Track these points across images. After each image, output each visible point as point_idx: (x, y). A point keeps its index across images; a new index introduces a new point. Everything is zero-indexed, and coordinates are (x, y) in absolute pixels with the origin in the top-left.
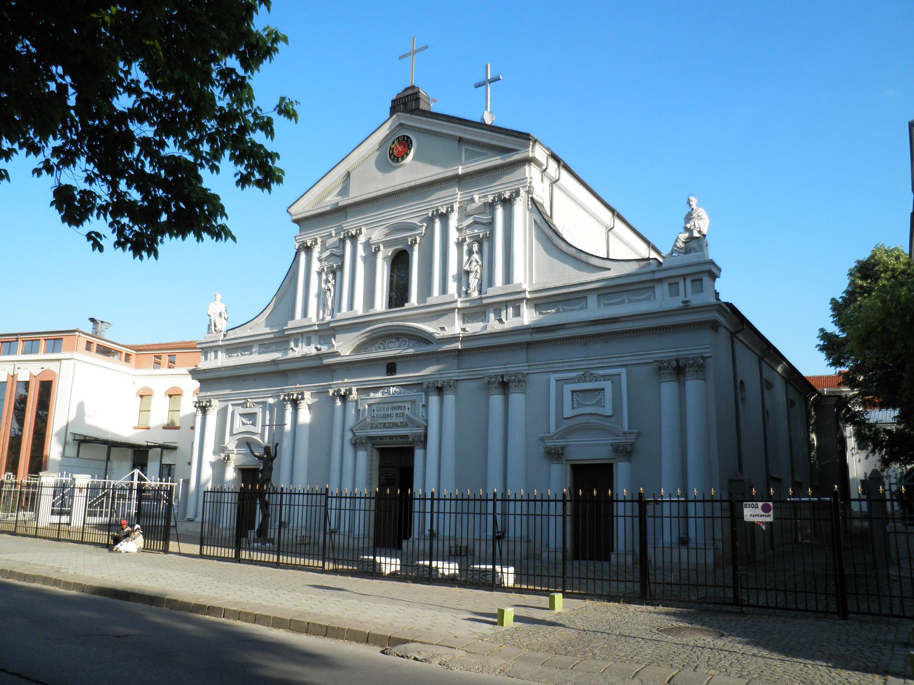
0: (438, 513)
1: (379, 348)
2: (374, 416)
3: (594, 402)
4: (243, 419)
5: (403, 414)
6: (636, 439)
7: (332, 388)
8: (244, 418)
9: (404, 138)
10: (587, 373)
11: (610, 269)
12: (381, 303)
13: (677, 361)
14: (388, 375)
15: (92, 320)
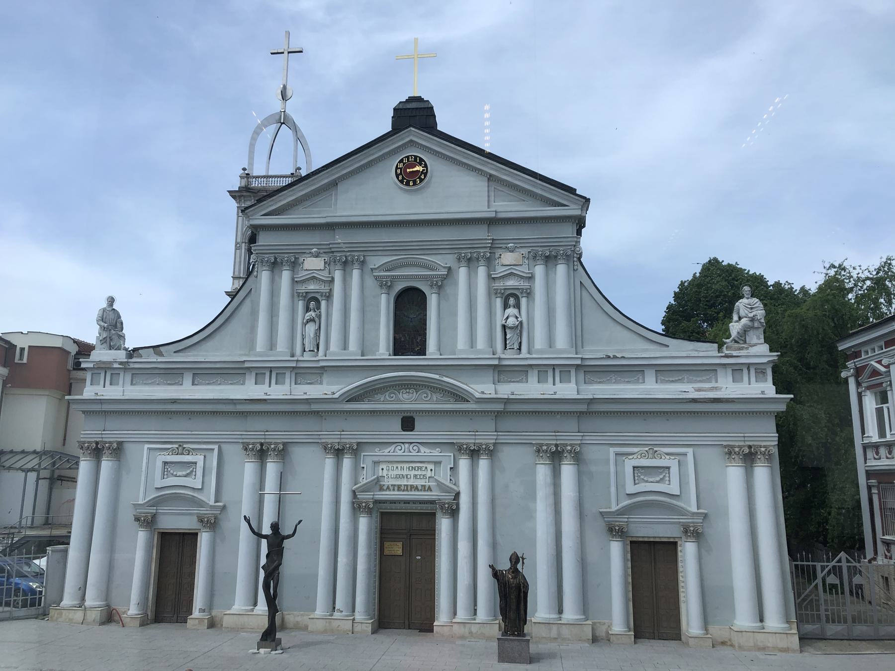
3: (658, 479)
6: (703, 520)
10: (651, 450)
11: (668, 346)
13: (262, 444)
15: (111, 301)
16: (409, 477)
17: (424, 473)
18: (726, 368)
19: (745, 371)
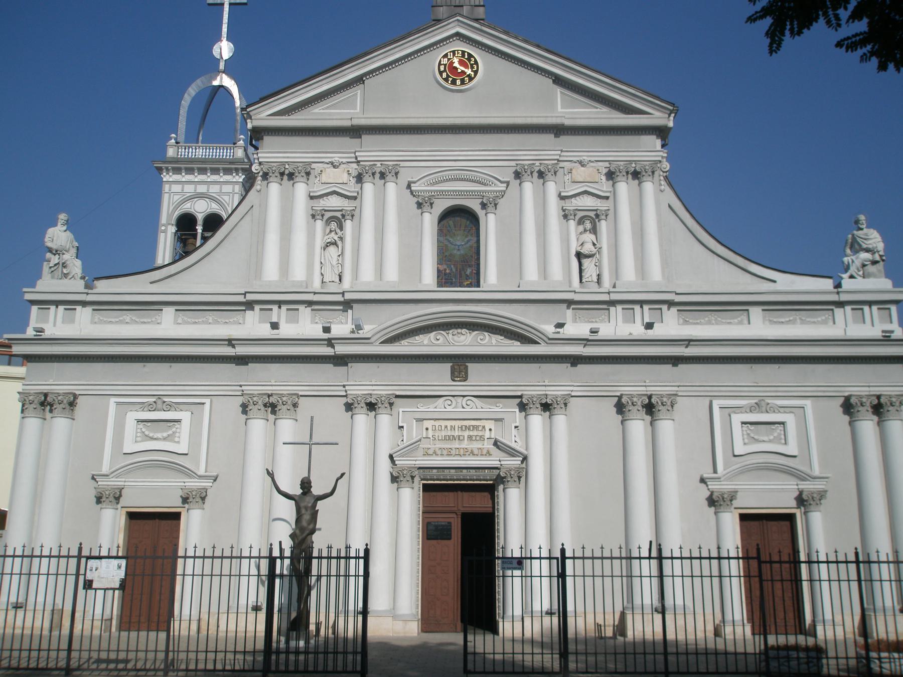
0: (329, 576)
3: (165, 435)
5: (481, 437)
17: (480, 433)
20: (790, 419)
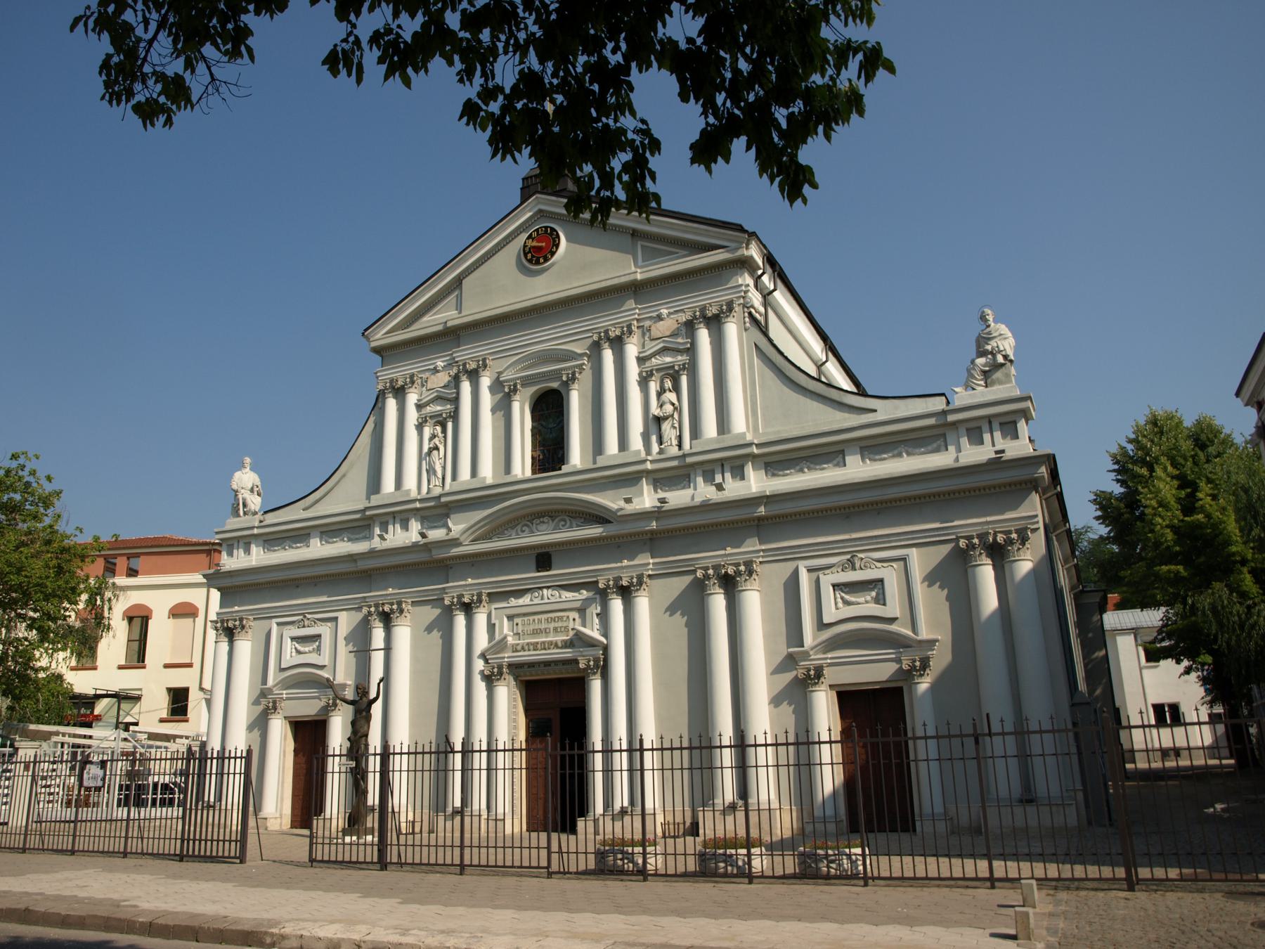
1: (523, 531)
2: (518, 634)
4: (297, 645)
5: (565, 627)
7: (447, 593)
8: (298, 643)
9: (546, 231)
11: (875, 411)
12: (522, 466)
14: (539, 571)
16: (548, 631)
17: (565, 624)
18: (957, 428)
19: (985, 427)
20: (891, 577)
